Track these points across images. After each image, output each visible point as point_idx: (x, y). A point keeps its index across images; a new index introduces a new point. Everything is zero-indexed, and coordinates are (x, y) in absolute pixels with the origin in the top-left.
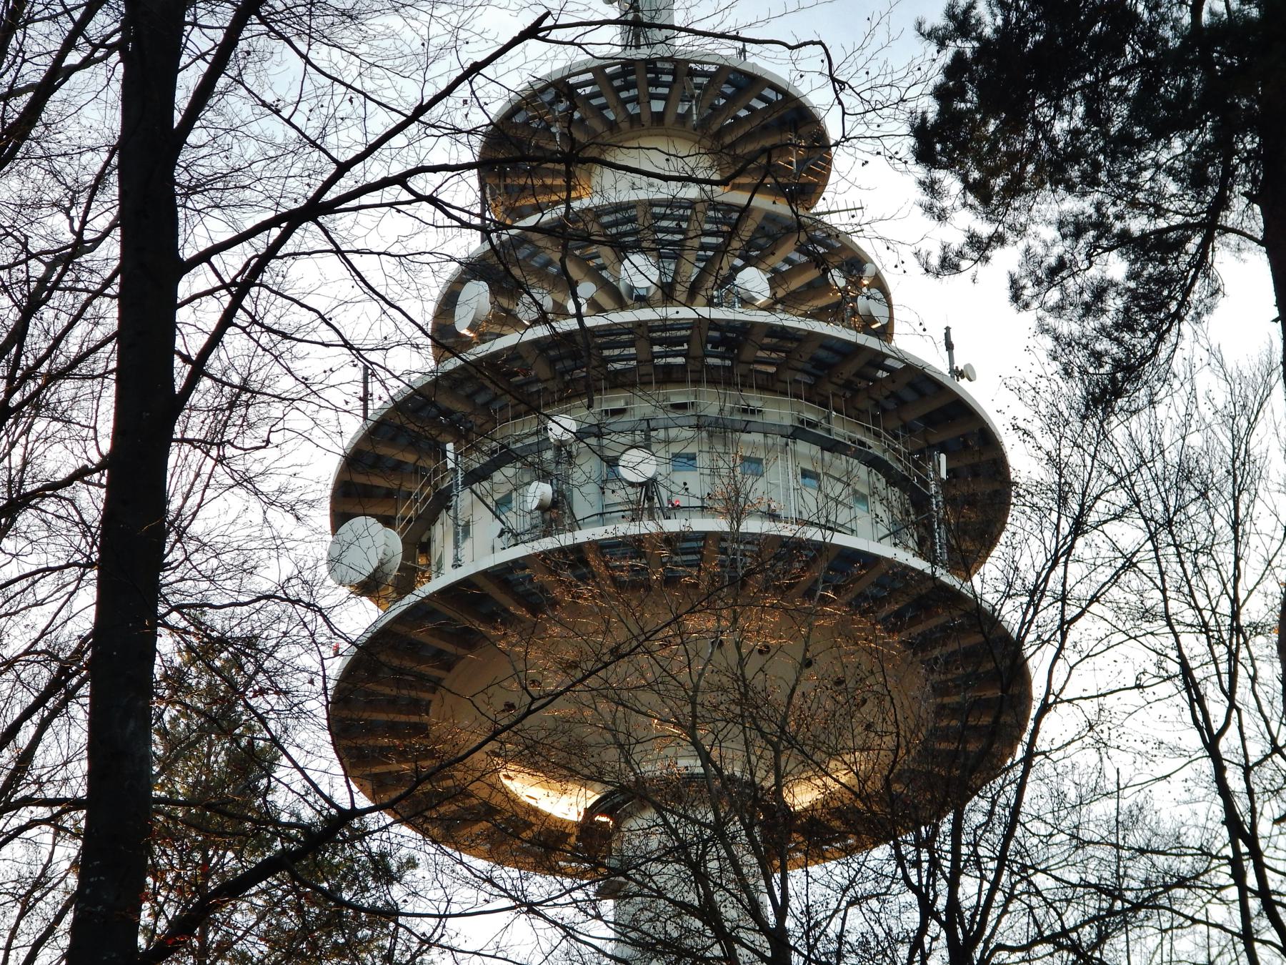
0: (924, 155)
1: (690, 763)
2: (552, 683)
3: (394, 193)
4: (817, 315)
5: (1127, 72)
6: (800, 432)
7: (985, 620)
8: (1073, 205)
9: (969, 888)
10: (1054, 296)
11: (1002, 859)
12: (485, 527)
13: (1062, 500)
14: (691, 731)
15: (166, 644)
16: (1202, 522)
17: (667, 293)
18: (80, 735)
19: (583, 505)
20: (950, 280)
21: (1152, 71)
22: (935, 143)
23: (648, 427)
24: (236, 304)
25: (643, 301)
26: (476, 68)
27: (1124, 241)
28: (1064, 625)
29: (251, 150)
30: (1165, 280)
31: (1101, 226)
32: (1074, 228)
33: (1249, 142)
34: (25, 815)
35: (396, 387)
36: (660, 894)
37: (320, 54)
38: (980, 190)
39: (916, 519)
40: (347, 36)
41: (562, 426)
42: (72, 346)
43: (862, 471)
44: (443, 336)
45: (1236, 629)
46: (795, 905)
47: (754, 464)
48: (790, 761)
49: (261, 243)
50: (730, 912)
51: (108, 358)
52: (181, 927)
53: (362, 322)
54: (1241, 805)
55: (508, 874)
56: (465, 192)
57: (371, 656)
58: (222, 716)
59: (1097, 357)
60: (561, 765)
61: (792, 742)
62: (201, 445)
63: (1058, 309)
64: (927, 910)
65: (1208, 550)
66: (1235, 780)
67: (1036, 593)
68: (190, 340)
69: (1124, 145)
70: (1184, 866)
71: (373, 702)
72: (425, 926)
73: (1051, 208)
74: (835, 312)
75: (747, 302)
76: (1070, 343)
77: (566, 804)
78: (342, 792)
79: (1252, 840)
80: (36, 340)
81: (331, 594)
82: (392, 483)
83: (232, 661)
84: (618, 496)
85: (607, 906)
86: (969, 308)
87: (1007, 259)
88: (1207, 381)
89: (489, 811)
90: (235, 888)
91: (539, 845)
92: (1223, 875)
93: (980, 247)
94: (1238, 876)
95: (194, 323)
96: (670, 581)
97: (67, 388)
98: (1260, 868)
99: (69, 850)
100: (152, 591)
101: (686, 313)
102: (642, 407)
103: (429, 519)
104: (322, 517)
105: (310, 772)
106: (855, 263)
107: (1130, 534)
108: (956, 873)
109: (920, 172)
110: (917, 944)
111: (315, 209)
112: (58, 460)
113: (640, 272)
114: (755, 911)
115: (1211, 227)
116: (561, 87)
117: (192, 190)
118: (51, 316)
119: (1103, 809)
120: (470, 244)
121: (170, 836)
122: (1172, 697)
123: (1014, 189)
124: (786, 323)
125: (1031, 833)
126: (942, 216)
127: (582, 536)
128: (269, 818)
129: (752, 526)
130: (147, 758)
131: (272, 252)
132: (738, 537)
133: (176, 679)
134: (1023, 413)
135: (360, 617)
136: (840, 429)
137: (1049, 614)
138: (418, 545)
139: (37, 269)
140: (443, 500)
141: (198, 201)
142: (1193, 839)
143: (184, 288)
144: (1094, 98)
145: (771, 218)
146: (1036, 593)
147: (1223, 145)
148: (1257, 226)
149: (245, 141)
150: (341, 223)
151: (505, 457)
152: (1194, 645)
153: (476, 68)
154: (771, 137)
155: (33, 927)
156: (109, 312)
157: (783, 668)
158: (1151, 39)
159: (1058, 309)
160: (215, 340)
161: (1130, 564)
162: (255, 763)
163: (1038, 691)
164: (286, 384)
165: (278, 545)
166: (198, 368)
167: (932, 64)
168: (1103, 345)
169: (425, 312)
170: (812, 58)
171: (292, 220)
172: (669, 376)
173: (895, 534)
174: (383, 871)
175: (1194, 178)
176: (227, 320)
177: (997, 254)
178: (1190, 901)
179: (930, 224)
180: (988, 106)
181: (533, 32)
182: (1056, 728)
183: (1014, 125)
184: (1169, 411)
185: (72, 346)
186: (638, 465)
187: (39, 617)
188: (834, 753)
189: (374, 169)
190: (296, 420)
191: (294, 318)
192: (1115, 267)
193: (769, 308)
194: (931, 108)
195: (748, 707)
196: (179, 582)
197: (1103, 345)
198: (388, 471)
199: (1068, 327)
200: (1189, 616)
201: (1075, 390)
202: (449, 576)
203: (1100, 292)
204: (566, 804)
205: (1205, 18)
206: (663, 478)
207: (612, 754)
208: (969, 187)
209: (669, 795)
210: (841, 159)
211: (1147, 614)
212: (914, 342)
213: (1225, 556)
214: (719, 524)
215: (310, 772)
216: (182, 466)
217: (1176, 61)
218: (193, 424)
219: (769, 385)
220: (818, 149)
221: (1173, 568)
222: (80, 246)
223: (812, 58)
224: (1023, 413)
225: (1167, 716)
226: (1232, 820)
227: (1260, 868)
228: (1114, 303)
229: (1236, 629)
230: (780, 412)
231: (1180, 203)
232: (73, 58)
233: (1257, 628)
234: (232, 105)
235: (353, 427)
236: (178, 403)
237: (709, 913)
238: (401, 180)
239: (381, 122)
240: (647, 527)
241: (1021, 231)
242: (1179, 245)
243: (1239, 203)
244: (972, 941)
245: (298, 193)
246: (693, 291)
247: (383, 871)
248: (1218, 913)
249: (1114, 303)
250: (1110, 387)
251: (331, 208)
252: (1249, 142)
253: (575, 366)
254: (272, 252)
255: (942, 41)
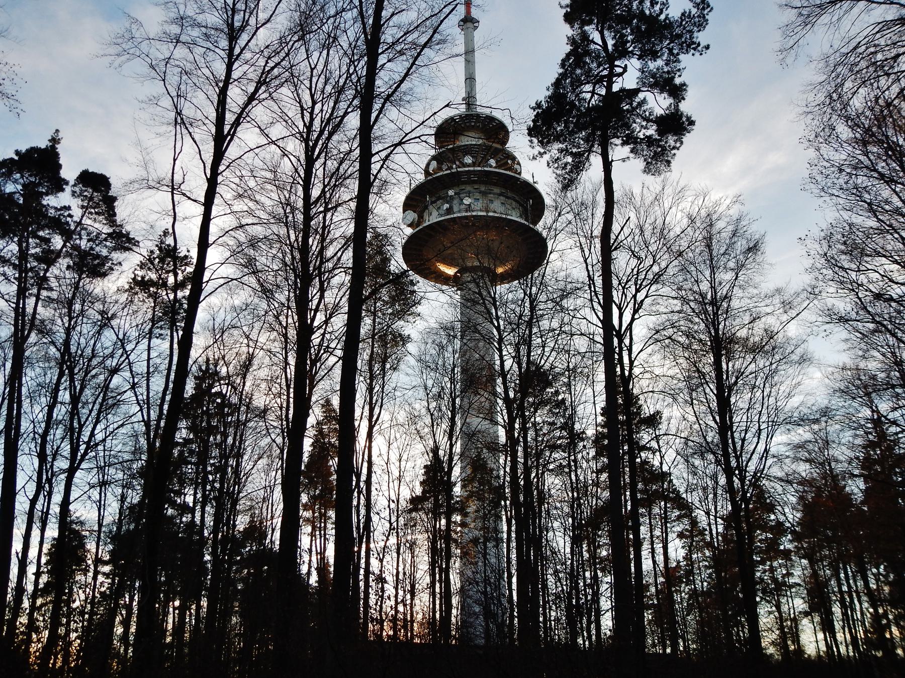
0: (530, 134)
1: (476, 263)
2: (449, 245)
3: (418, 140)
4: (505, 170)
5: (573, 118)
6: (501, 194)
7: (539, 235)
8: (561, 146)
9: (534, 289)
10: (556, 165)
11: (541, 283)
12: (435, 213)
13: (556, 209)
14: (477, 256)
15: (368, 235)
16: (584, 214)
17: (474, 164)
18: (351, 254)
19: (455, 209)
20: (534, 161)
21: (578, 117)
22: (532, 132)
23: (469, 192)
24: (384, 163)
25: (469, 166)
26: (435, 113)
27: (572, 154)
28: (556, 236)
29: (387, 130)
30: (580, 162)
31: (567, 150)
32: (561, 151)
33: (599, 133)
34: (339, 270)
35: (417, 182)
36: (470, 289)
37: (402, 109)
38: (541, 143)
39: (524, 214)
40: (407, 106)
41: (451, 193)
42: (349, 172)
43: (514, 203)
44: (427, 172)
45: (592, 237)
46: (498, 292)
47: (492, 201)
48: (498, 263)
49: (389, 151)
50: (485, 293)
51: (357, 175)
52: (371, 294)
53: (411, 168)
54: (591, 273)
55: (438, 285)
56: (432, 140)
57: (411, 239)
58: (380, 251)
59: (565, 179)
60: (450, 264)
61: (498, 259)
62: (376, 194)
63: (557, 168)
64: (525, 294)
65: (586, 220)
66: (590, 268)
67: (550, 229)
68: (374, 172)
69: (572, 133)
70: (579, 286)
71: (411, 249)
72: (422, 294)
73: (557, 146)
74: (510, 169)
75: (491, 166)
76: (559, 176)
77: (451, 271)
78: (405, 267)
79: (593, 281)
80: (341, 171)
81: (403, 226)
82: (415, 203)
83: (382, 239)
84: (463, 207)
85: (459, 292)
86: (537, 168)
87: (547, 157)
88: (588, 184)
89: (435, 273)
90: (382, 286)
91: (443, 279)
92: (587, 288)
93: (541, 154)
94: (590, 288)
95: (375, 168)
96: (473, 225)
97: (348, 181)
98: (594, 287)
99: (349, 278)
100: (366, 224)
101: (479, 169)
102: (468, 188)
103: (423, 211)
104: (401, 209)
105: (397, 263)
106: (514, 158)
107: (570, 216)
108: (532, 286)
109: (529, 138)
110: (523, 301)
111: (400, 143)
112: (346, 197)
113: (468, 160)
114: (489, 293)
115: (590, 151)
116: (452, 119)
117: (375, 139)
118: (344, 166)
119: (563, 274)
120: (433, 152)
121: (368, 275)
122: (577, 252)
123: (548, 142)
124: (358, 396)
125: (548, 277)
126: (533, 147)
127: (455, 215)
128: (389, 272)
129: (491, 214)
130: (365, 259)
131: (391, 153)
132: (487, 216)
133: (371, 244)
134: (549, 190)
135: (409, 231)
136: (509, 194)
137: (552, 233)
138: (421, 217)
139: (342, 156)
140: (426, 208)
141: (376, 142)
142: (581, 280)
143: (373, 160)
144: (566, 122)
145: (496, 148)
146: (550, 229)
147: (593, 133)
148: (600, 151)
149: (387, 126)
150: (405, 146)
151: (439, 198)
152: (583, 240)
153: (435, 113)
154: (495, 131)
155: (341, 293)
156: (357, 165)
157: (496, 244)
158: (579, 110)
159: (557, 168)
160: (379, 171)
161: (570, 223)
162: (386, 261)
163: (549, 249)
164: (394, 181)
165: (392, 215)
166: (376, 177)
167: (532, 114)
168: (566, 176)
169: (423, 166)
170: (507, 112)
171: (396, 145)
172: (474, 182)
173: (521, 216)
174: (412, 283)
175: (586, 140)
176: (382, 167)
177: (544, 156)
178: (580, 293)
179: (530, 149)
180: (543, 124)
181: (447, 106)
182: (553, 257)
183: (548, 129)
184: (580, 190)
185: (349, 172)
186: (467, 201)
187: (342, 230)
188: (507, 261)
189: (413, 135)
190: (396, 189)
191: (396, 167)
192: (569, 159)
193: (495, 168)
194: (532, 124)
195: (489, 252)
196: (372, 221)
197: (566, 176)
198: (415, 201)
199: (559, 172)
200: (582, 234)
201: (560, 186)
202: (427, 223)
203: (566, 164)
204: (451, 271)
205: (662, 17)
206: (472, 205)
207: (460, 261)
208: (539, 141)
209: (473, 269)
210: (512, 135)
211: (573, 233)
212: (526, 176)
213: (590, 221)
214: (484, 214)
215: (397, 263)
216: (372, 198)
217: (583, 115)
218: (375, 190)
219: (495, 185)
220: (507, 133)
221: (579, 224)
222: (351, 151)
223: (507, 112)
224: (549, 190)
225: (576, 254)
226: (589, 276)
227: (594, 287)
228: (569, 167)
229: (592, 237)
230: (497, 190)
231: (583, 146)
232: (349, 110)
233: (596, 237)
234: (383, 121)
235: (408, 191)
236: (371, 185)
237: (480, 294)
238: (419, 137)
239: (415, 125)
240: (469, 214)
241: (550, 151)
242: (583, 155)
243: (596, 146)
244: (534, 300)
245: (397, 140)
246: (480, 163)
247: (412, 283)
248: (586, 296)
249: (569, 167)
250: (567, 184)
251: (404, 143)
252: (599, 133)
253: (454, 180)
254: (391, 153)
255: (534, 109)
